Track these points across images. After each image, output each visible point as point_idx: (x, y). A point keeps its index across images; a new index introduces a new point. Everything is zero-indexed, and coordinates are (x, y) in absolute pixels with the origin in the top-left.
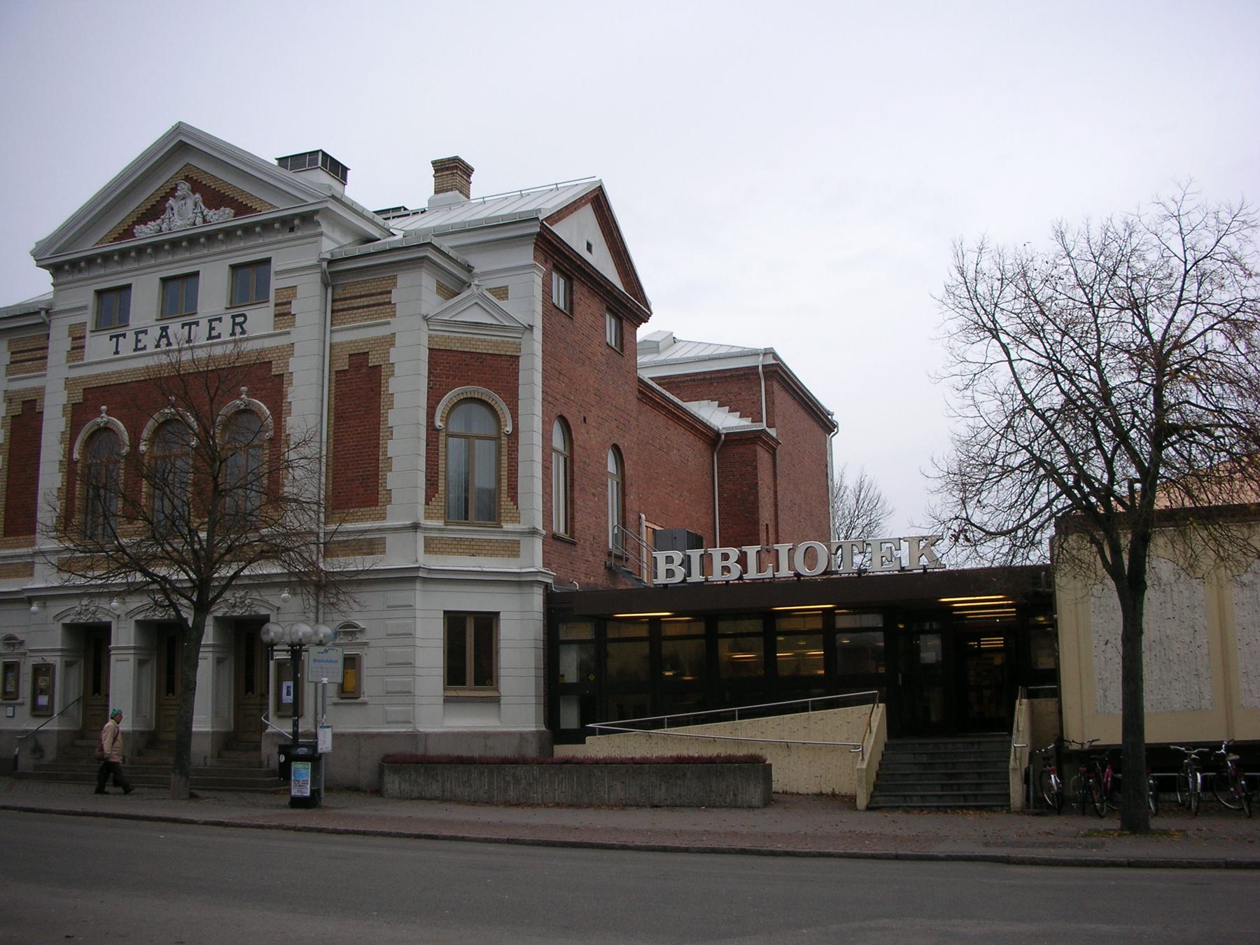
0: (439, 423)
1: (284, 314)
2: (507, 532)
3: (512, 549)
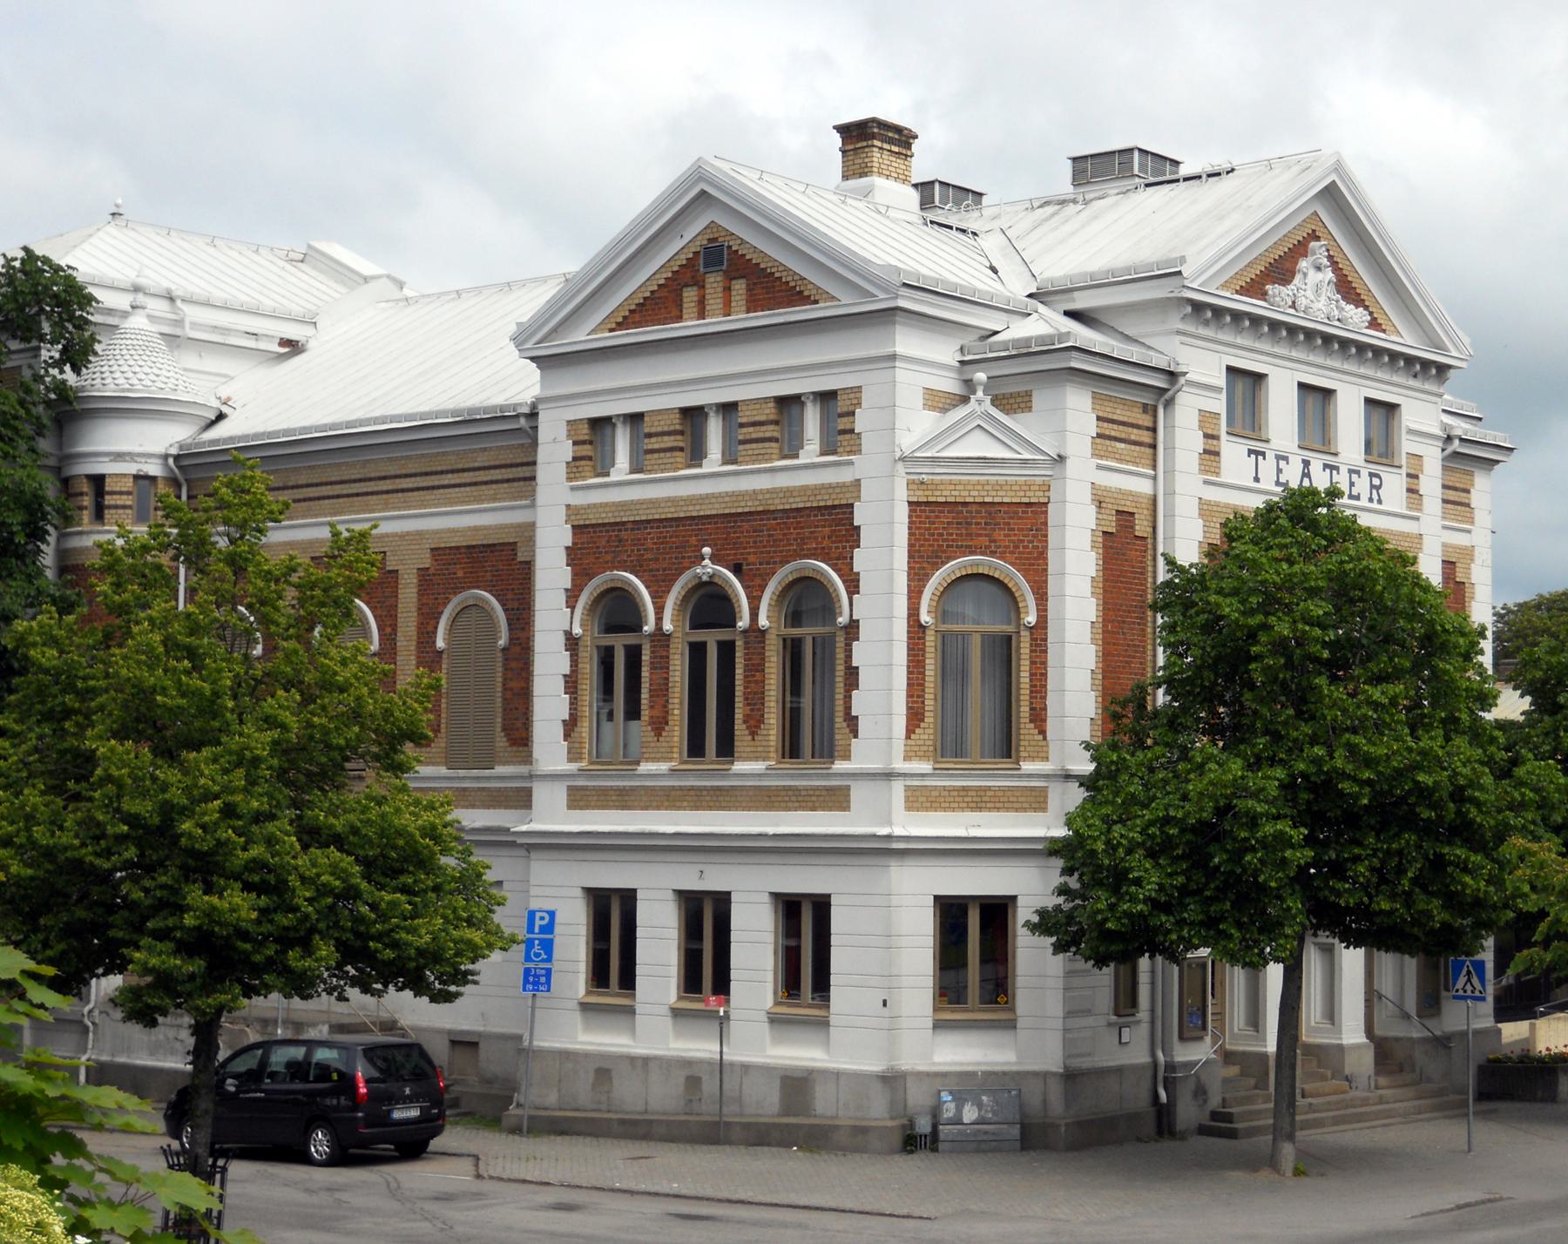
0: (925, 618)
2: (1030, 776)
3: (1035, 801)
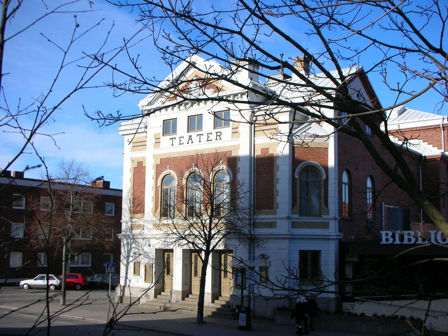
0: (297, 177)
1: (236, 132)
2: (324, 219)
3: (326, 226)
